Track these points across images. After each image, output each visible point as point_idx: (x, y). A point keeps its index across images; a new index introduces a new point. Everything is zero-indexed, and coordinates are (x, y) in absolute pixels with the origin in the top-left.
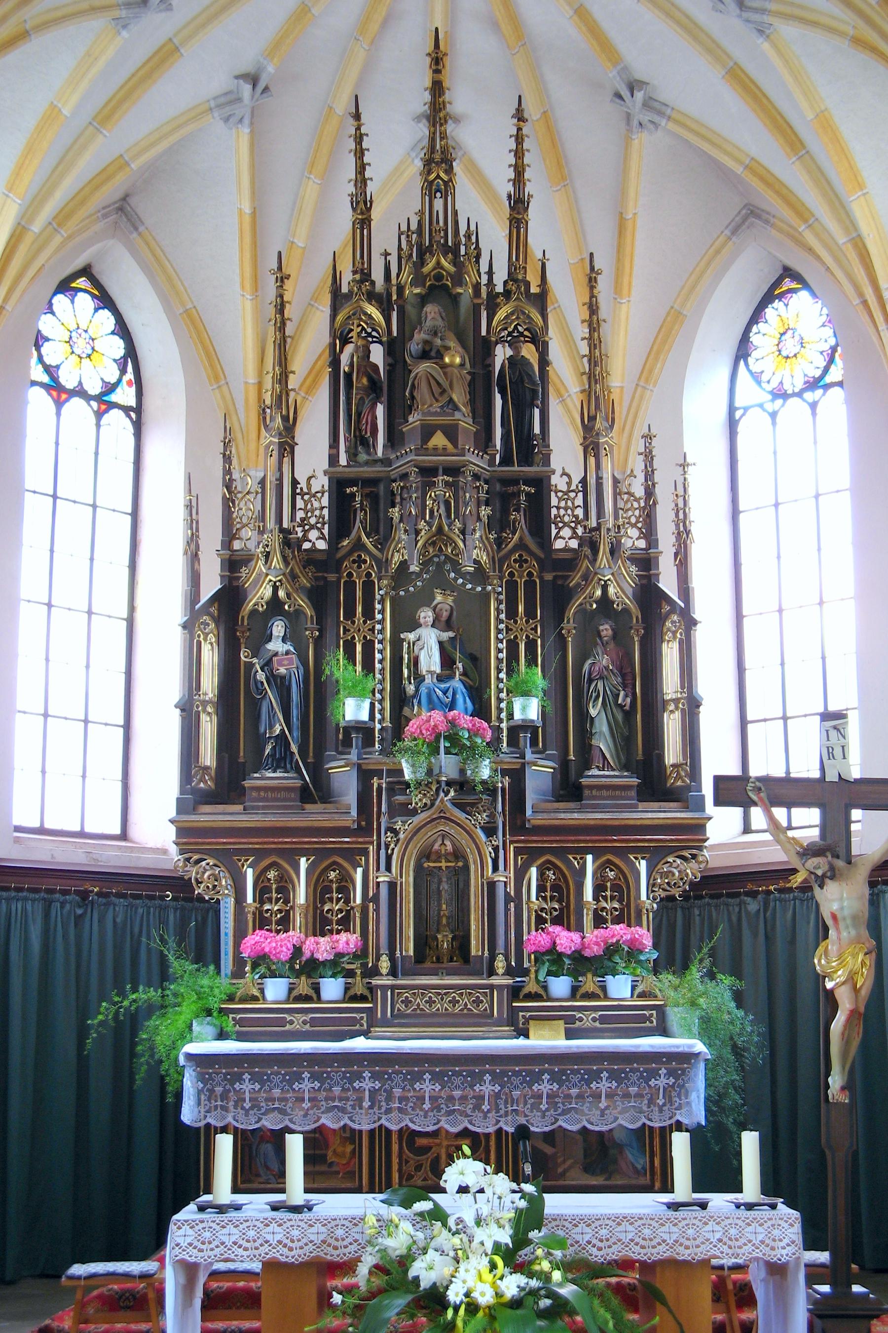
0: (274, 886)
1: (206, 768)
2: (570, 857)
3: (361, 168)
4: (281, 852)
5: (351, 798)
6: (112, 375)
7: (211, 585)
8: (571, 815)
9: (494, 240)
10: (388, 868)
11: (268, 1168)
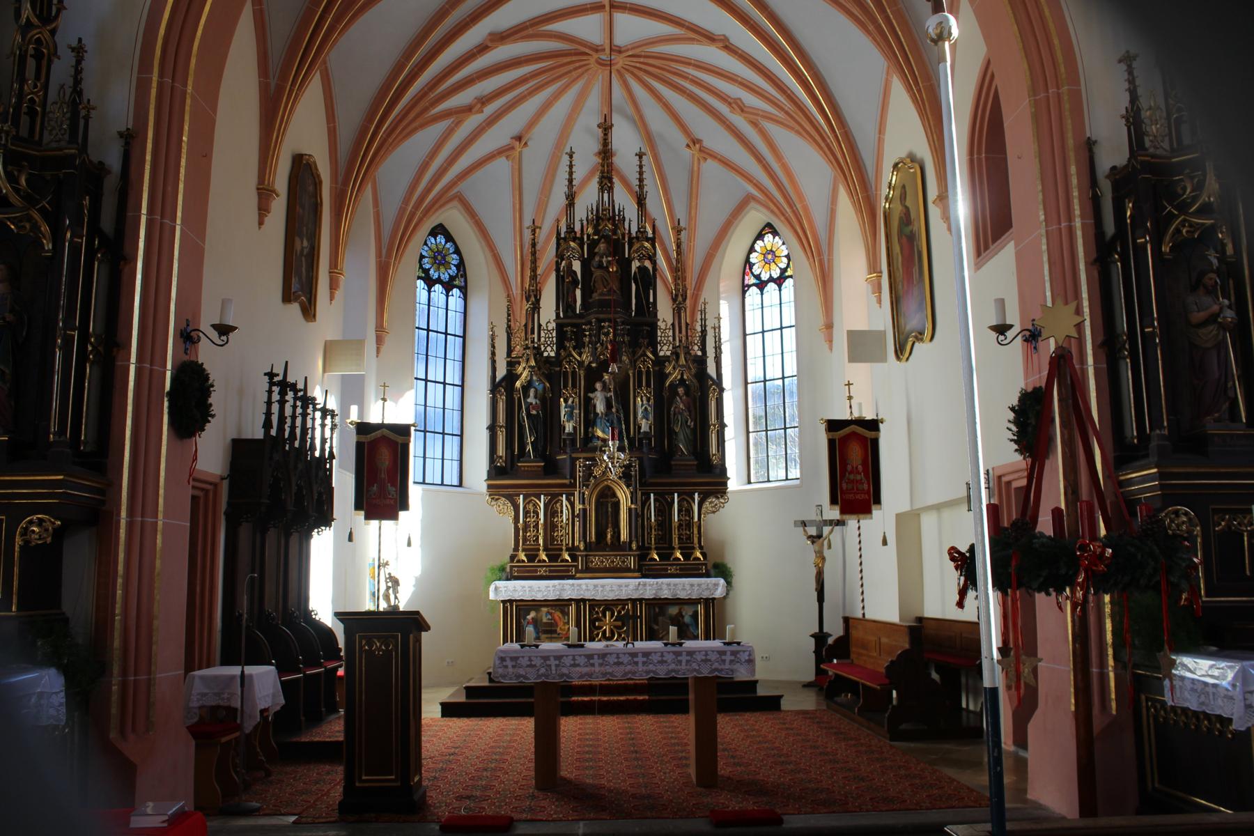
3: (571, 173)
4: (535, 495)
5: (567, 472)
7: (501, 372)
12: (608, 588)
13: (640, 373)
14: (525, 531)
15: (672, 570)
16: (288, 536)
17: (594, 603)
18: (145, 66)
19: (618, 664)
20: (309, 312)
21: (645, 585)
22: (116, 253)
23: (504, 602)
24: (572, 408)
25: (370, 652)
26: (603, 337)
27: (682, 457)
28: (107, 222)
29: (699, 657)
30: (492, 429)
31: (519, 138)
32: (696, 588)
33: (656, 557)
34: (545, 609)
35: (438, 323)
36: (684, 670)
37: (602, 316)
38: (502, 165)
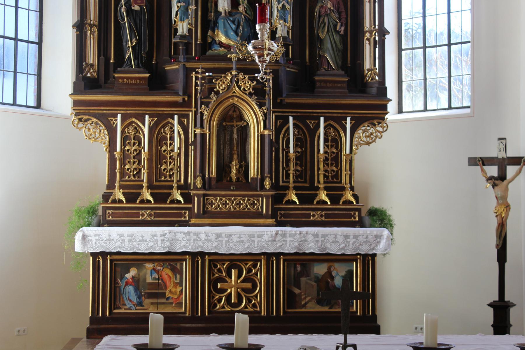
0: (132, 136)
1: (92, 66)
2: (308, 122)
5: (179, 86)
10: (202, 127)
11: (130, 301)
12: (235, 239)
14: (123, 163)
15: (316, 216)
17: (215, 259)
21: (284, 235)
30: (80, 27)
32: (351, 240)
33: (295, 199)
34: (149, 266)
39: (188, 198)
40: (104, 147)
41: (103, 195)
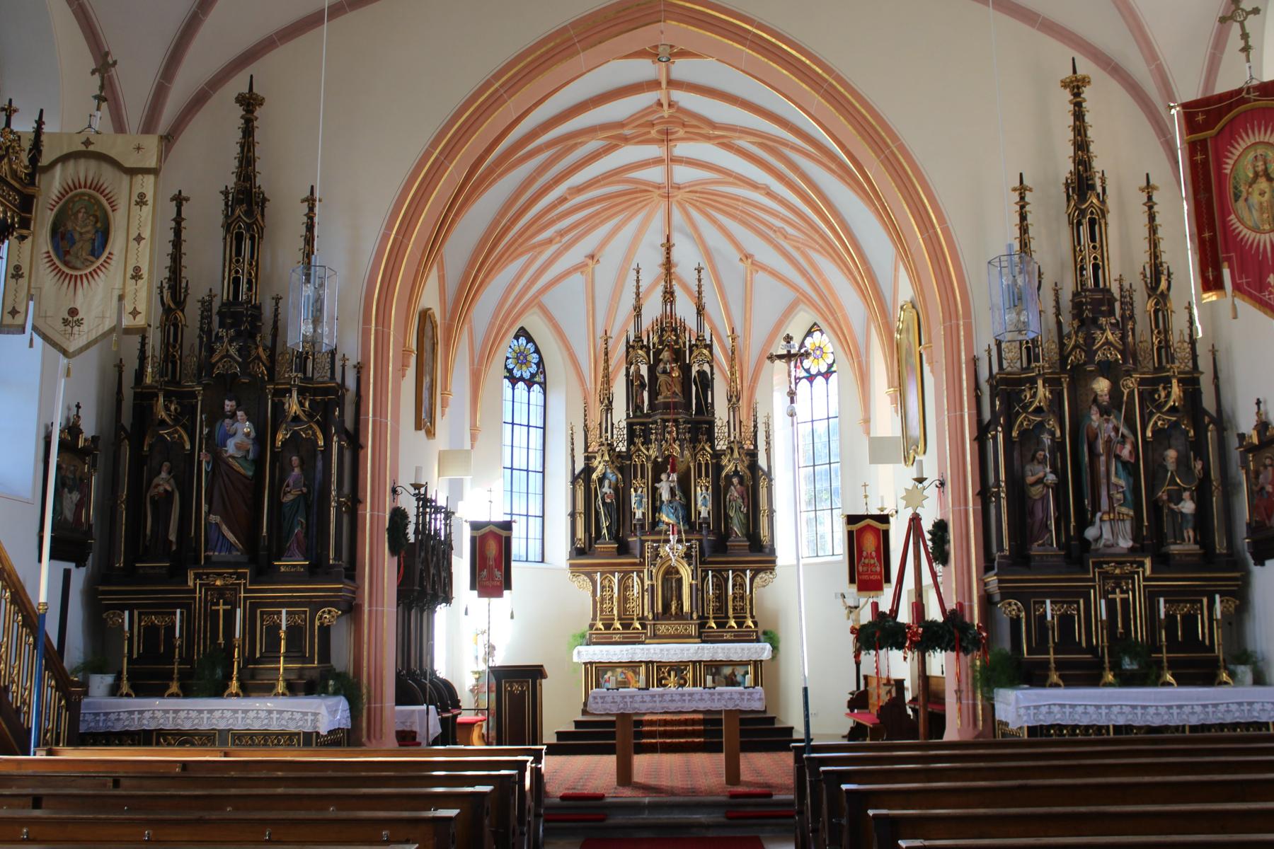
5: (637, 552)
6: (534, 369)
7: (580, 465)
8: (700, 418)
9: (691, 323)
13: (700, 465)
14: (602, 603)
15: (727, 636)
16: (422, 611)
17: (660, 665)
18: (367, 320)
19: (672, 701)
20: (431, 433)
22: (354, 441)
23: (586, 664)
24: (642, 498)
25: (511, 692)
26: (667, 436)
27: (734, 539)
28: (349, 424)
29: (727, 696)
31: (592, 257)
34: (619, 670)
35: (521, 418)
36: (716, 706)
37: (666, 417)
38: (577, 278)
39: (644, 626)
40: (590, 594)
41: (481, 595)
